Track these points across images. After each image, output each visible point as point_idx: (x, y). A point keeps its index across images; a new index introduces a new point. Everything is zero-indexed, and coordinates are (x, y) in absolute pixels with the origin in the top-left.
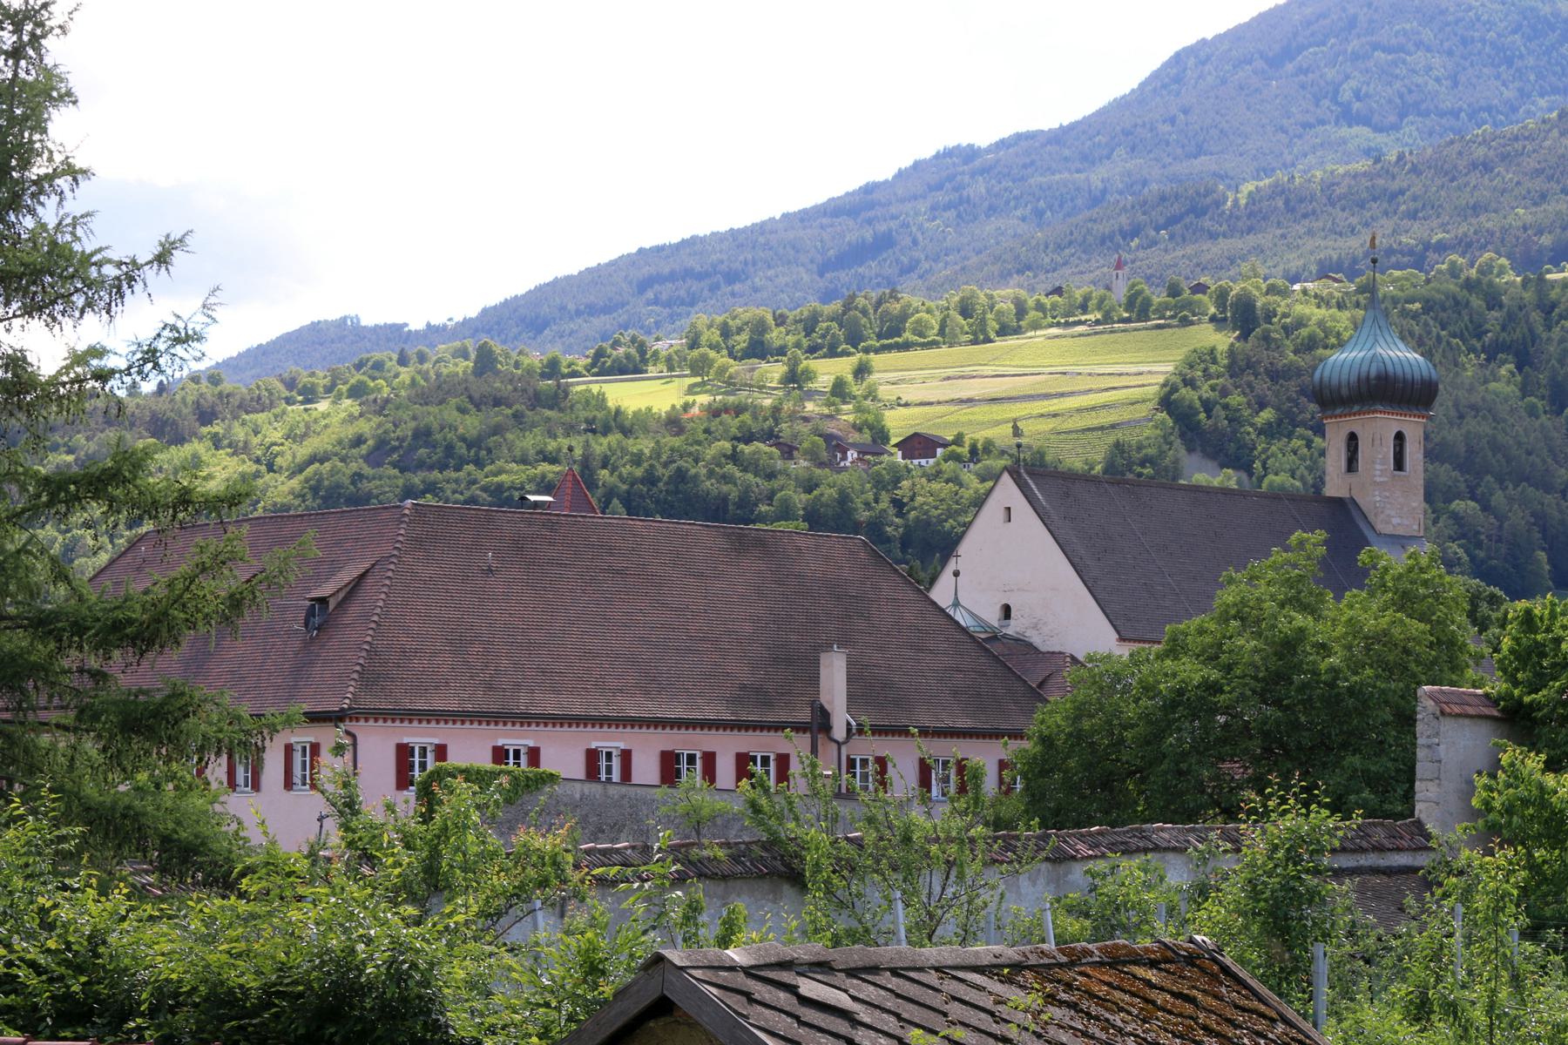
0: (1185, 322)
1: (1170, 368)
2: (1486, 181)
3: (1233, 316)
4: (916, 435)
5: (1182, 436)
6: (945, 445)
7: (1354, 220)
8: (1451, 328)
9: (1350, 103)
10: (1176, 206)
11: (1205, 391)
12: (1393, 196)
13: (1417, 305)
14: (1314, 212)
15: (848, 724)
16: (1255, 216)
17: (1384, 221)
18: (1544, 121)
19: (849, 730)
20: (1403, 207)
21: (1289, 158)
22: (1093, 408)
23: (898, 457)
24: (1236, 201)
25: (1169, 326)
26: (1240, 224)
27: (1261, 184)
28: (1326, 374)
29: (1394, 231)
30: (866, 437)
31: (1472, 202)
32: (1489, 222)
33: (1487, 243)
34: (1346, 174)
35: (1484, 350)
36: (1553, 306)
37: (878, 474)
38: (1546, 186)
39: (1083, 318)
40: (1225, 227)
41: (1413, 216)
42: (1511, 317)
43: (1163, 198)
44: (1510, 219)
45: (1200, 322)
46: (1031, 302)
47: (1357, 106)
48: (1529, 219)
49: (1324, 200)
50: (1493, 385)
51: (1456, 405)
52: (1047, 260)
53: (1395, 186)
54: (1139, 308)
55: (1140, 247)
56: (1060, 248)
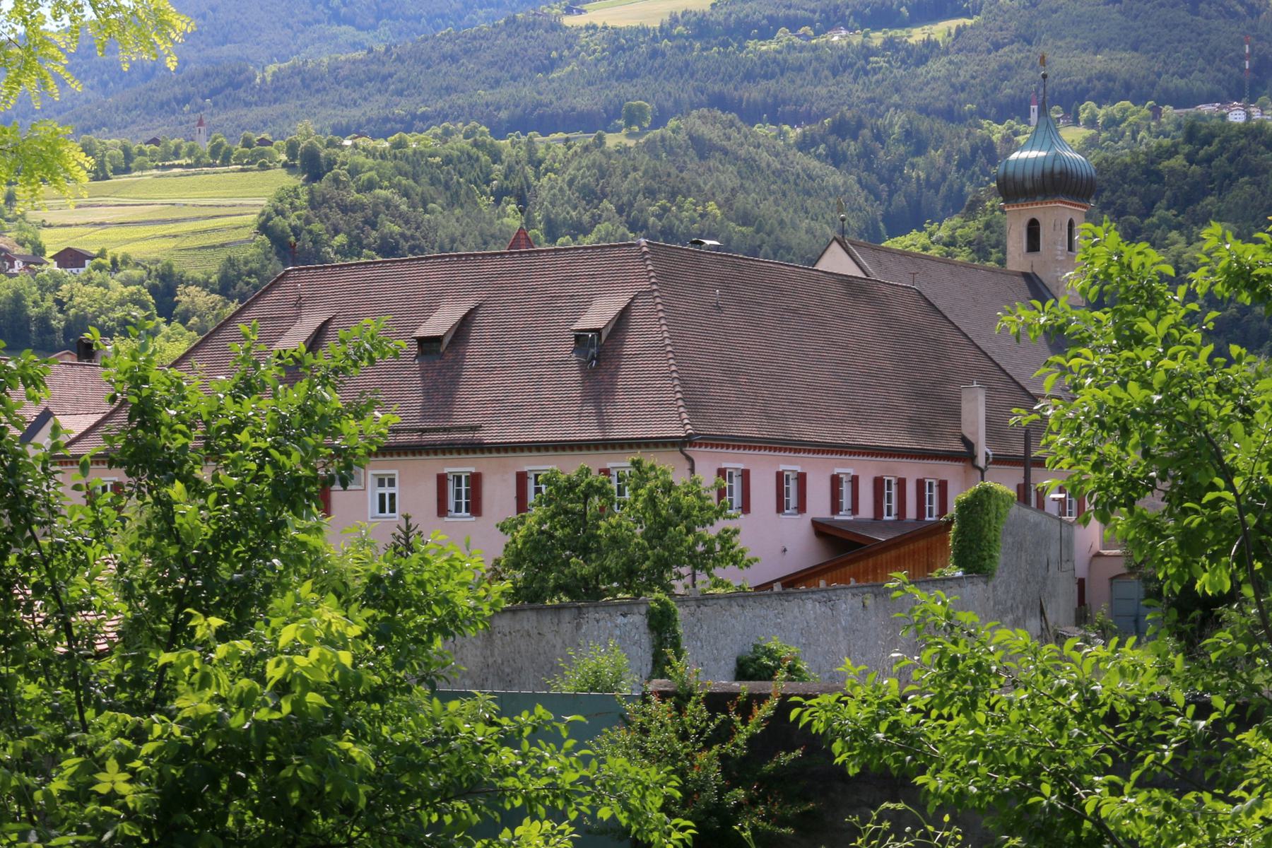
0: (264, 167)
1: (264, 202)
2: (454, 70)
3: (302, 164)
4: (69, 249)
5: (277, 254)
6: (92, 258)
7: (355, 95)
8: (467, 176)
9: (338, 8)
10: (217, 81)
11: (293, 219)
12: (384, 79)
13: (438, 159)
14: (324, 89)
16: (279, 90)
17: (378, 97)
18: (494, 26)
19: (987, 459)
20: (392, 87)
21: (294, 48)
22: (205, 231)
23: (54, 266)
24: (263, 80)
25: (251, 170)
26: (268, 96)
27: (282, 66)
29: (387, 105)
30: (28, 250)
31: (445, 85)
32: (459, 100)
33: (459, 116)
34: (347, 61)
35: (492, 194)
36: (540, 162)
37: (43, 279)
38: (499, 75)
39: (177, 162)
40: (256, 97)
41: (400, 93)
42: (510, 169)
43: (207, 75)
44: (475, 98)
45: (275, 167)
46: (135, 150)
47: (343, 10)
48: (489, 98)
49: (332, 79)
50: (506, 220)
51: (481, 234)
52: (119, 119)
53: (385, 70)
54: (221, 156)
55: (191, 111)
56: (128, 110)
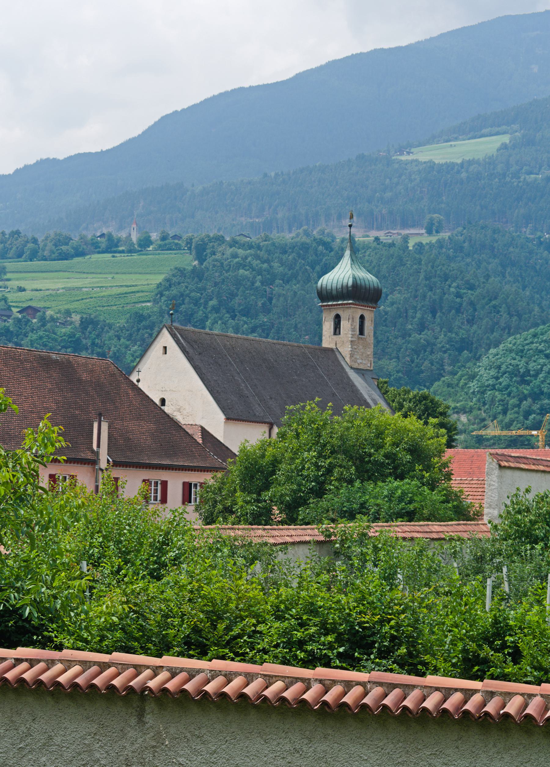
15: (108, 460)
28: (324, 283)
